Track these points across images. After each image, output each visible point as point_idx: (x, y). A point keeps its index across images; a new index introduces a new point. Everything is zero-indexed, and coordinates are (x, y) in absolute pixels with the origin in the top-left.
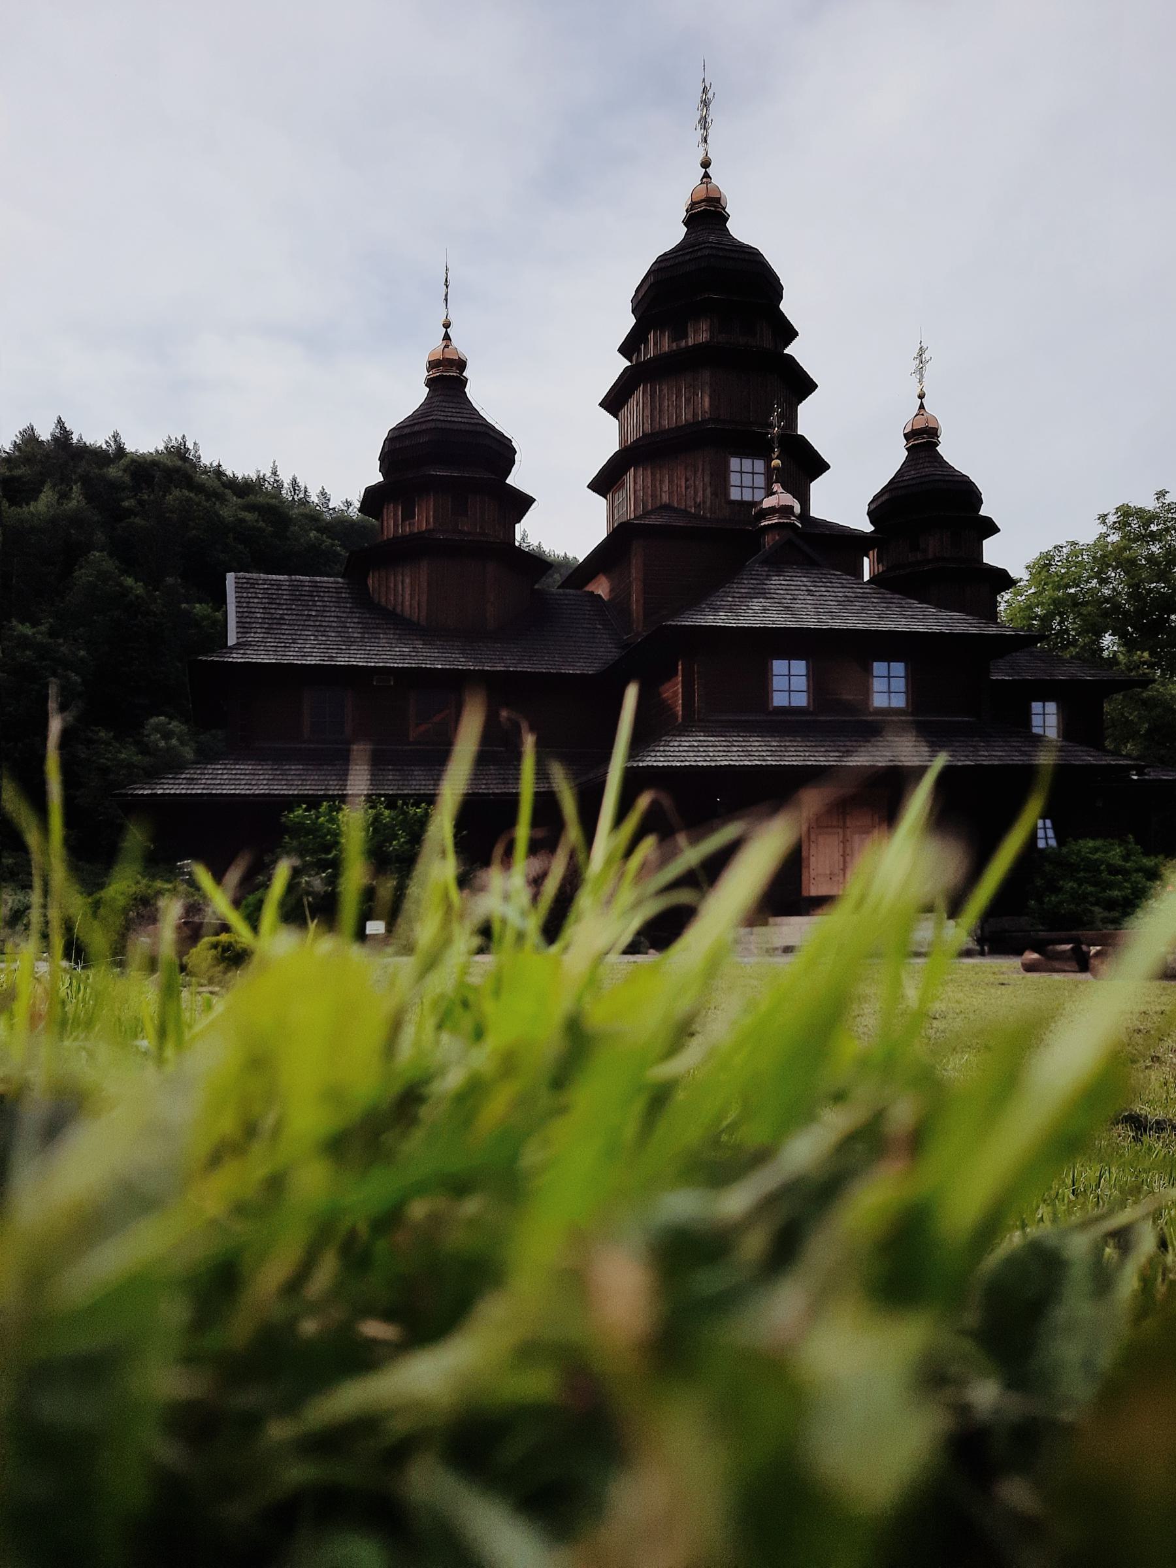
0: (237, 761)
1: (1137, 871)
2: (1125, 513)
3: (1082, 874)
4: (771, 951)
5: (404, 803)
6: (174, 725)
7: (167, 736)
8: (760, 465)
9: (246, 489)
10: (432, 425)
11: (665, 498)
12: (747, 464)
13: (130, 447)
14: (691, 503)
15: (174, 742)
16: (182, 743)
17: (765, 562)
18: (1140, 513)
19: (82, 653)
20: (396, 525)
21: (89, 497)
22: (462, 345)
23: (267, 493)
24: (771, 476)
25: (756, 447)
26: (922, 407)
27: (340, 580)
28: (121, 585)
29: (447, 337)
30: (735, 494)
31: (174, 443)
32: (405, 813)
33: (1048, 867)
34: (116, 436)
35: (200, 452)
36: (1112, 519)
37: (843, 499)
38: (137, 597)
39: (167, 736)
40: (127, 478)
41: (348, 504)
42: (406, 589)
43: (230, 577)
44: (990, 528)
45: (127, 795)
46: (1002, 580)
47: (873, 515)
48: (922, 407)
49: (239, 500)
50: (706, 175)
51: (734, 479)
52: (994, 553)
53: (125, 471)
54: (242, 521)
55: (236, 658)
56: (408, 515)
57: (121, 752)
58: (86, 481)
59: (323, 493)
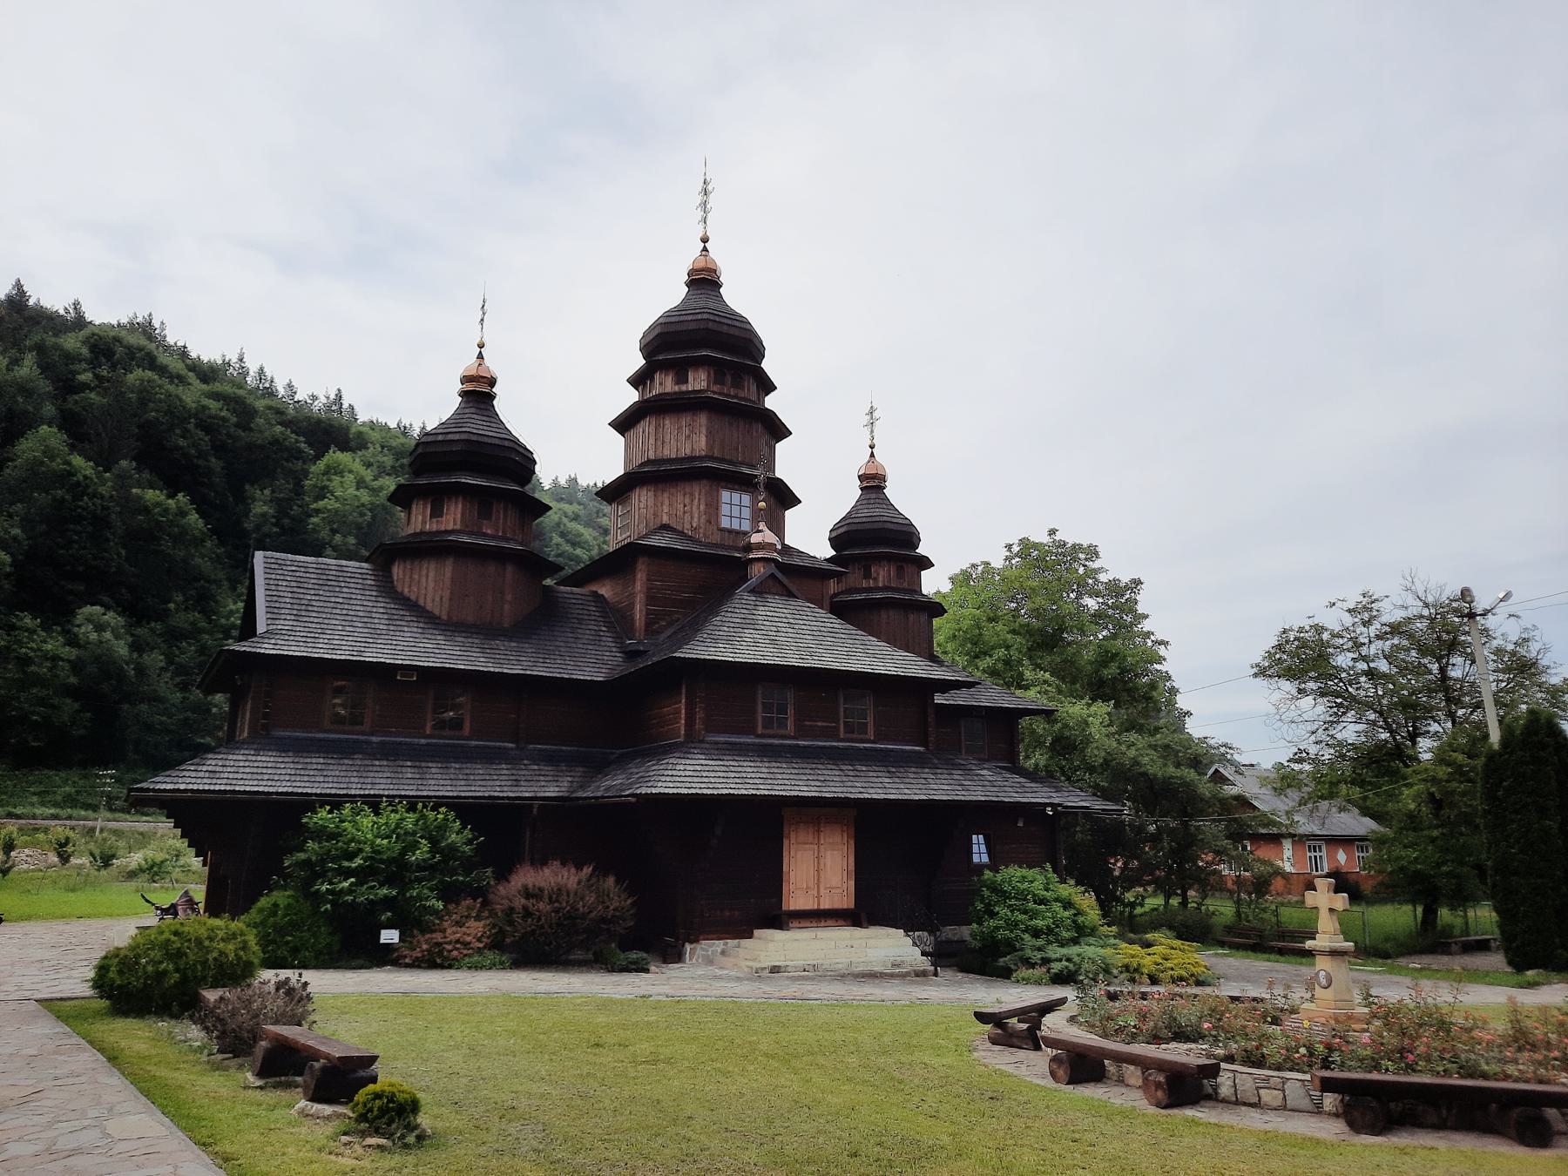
0: (258, 751)
1: (1056, 900)
2: (1026, 544)
3: (1013, 902)
4: (757, 975)
5: (425, 806)
6: (111, 617)
7: (100, 628)
8: (746, 499)
9: (208, 373)
10: (464, 437)
11: (665, 520)
12: (736, 496)
13: (89, 317)
14: (687, 526)
15: (108, 635)
16: (117, 637)
17: (752, 591)
18: (1036, 546)
19: (16, 531)
20: (424, 522)
21: (45, 367)
22: (493, 365)
23: (232, 382)
24: (756, 516)
25: (744, 483)
26: (872, 455)
27: (365, 565)
28: (68, 463)
29: (480, 356)
30: (725, 523)
31: (140, 320)
32: (423, 817)
33: (986, 893)
34: (76, 305)
35: (166, 332)
36: (1016, 549)
37: (809, 533)
38: (86, 477)
39: (100, 628)
40: (85, 351)
41: (314, 398)
42: (429, 582)
43: (259, 557)
44: (925, 563)
45: (148, 790)
46: (934, 608)
47: (835, 541)
48: (872, 455)
49: (204, 387)
50: (705, 249)
51: (725, 509)
52: (933, 583)
53: (84, 343)
54: (204, 408)
55: (267, 648)
56: (437, 513)
57: (45, 642)
58: (40, 349)
59: (290, 386)
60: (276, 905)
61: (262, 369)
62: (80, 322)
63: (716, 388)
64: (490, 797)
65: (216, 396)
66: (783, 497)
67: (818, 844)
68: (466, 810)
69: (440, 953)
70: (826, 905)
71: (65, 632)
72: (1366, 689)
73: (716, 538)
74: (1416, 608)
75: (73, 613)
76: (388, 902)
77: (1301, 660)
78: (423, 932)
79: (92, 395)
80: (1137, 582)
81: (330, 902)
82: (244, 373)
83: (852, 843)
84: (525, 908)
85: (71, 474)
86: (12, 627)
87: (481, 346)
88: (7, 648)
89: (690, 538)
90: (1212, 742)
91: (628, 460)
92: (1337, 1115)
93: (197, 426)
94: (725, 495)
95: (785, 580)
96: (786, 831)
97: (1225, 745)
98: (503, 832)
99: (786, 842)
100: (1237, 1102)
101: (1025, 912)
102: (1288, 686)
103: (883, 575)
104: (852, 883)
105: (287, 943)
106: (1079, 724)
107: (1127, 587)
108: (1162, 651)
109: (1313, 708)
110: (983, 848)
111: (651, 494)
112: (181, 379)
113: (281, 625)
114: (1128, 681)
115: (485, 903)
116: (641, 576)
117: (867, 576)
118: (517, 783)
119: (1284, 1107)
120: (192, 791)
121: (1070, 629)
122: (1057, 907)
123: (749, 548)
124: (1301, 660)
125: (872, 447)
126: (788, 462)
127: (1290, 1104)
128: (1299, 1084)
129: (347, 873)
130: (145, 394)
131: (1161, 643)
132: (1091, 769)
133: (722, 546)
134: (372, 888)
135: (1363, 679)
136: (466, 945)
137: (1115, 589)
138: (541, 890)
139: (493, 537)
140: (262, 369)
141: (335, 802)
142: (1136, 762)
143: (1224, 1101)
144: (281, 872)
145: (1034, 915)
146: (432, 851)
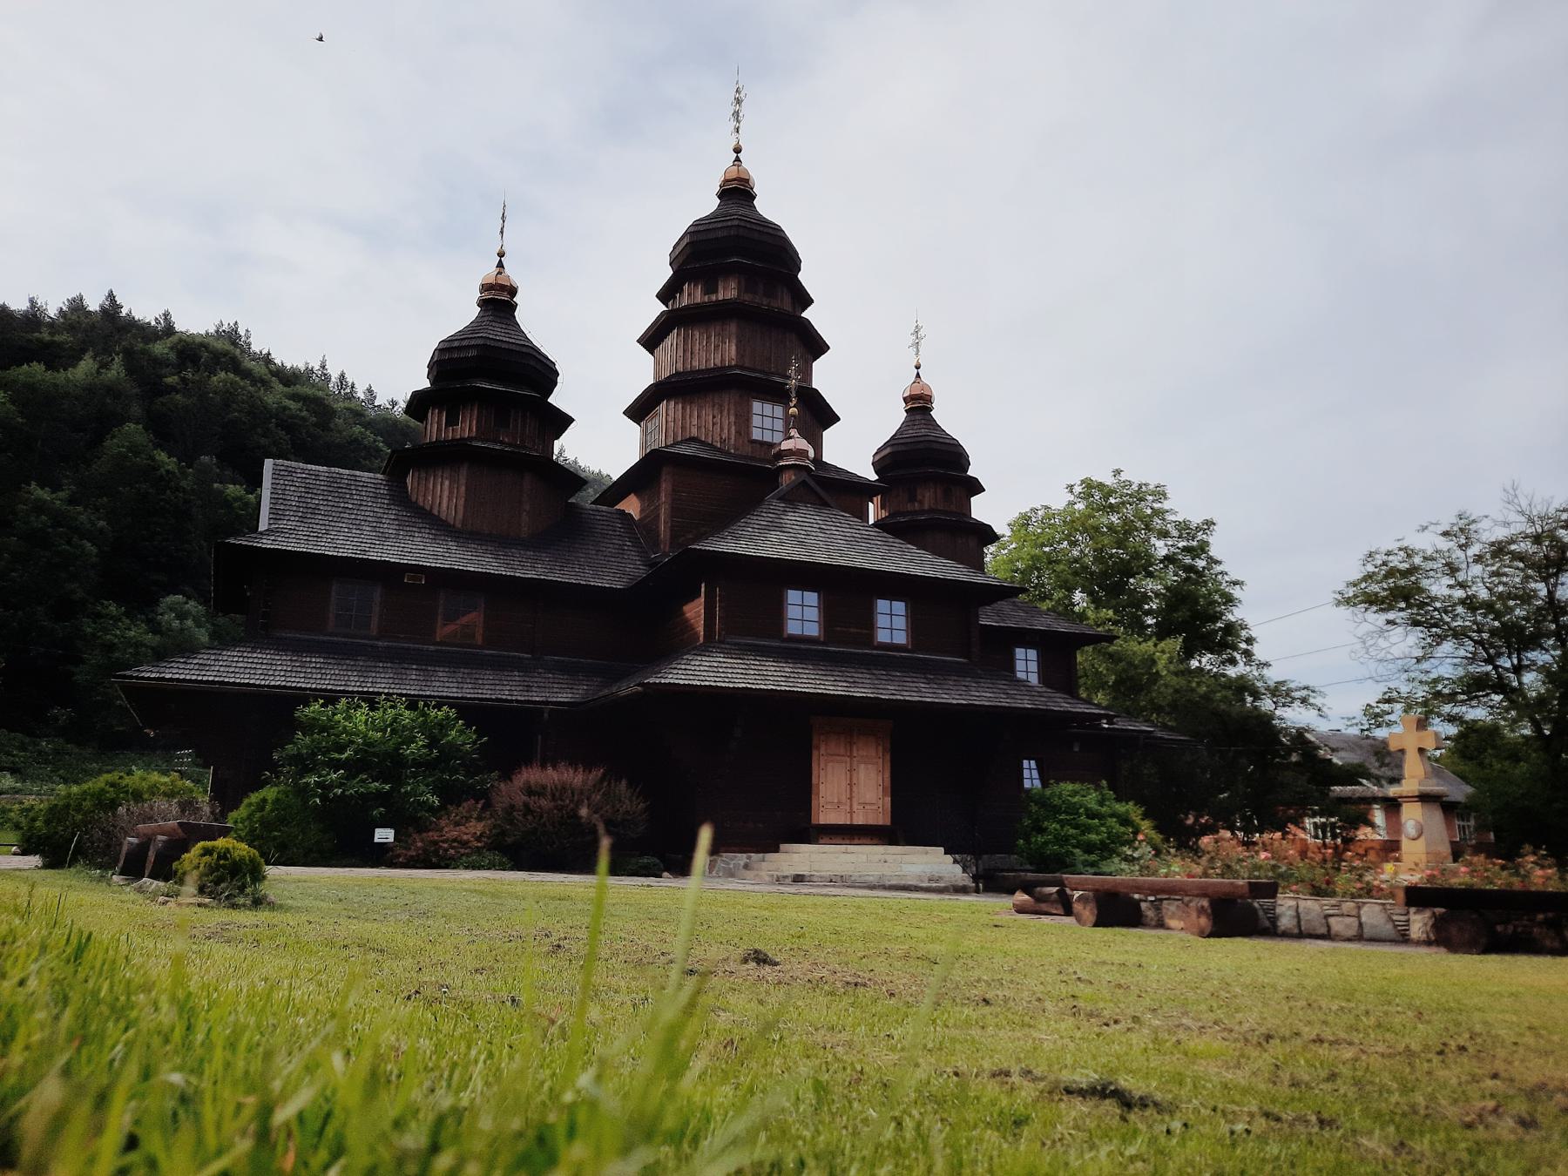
1: (1112, 816)
2: (1089, 485)
6: (192, 606)
9: (289, 378)
10: (479, 342)
11: (694, 432)
12: (768, 408)
13: (179, 327)
15: (189, 623)
17: (782, 499)
19: (102, 523)
22: (514, 274)
25: (777, 394)
26: (918, 375)
27: (379, 476)
28: (152, 458)
29: (500, 265)
30: (756, 435)
31: (225, 327)
32: (424, 715)
34: (166, 315)
36: (1078, 489)
37: (853, 448)
39: (182, 616)
40: (172, 356)
41: (394, 403)
42: (444, 493)
43: (268, 464)
45: (131, 677)
46: (986, 535)
47: (878, 466)
48: (918, 375)
50: (738, 159)
51: (756, 421)
52: (980, 509)
53: (171, 348)
54: (285, 408)
55: (266, 543)
56: (452, 421)
58: (129, 354)
59: (370, 391)
60: (264, 800)
61: (342, 376)
62: (169, 330)
63: (747, 297)
64: (497, 700)
65: (295, 397)
66: (818, 415)
67: (851, 757)
68: (469, 711)
69: (436, 853)
70: (859, 820)
71: (149, 621)
72: (1463, 618)
73: (748, 450)
74: (1520, 526)
75: (156, 603)
76: (380, 797)
77: (1394, 590)
78: (419, 832)
79: (178, 397)
80: (1209, 523)
81: (320, 796)
82: (327, 378)
83: (888, 757)
84: (526, 805)
85: (156, 469)
86: (99, 615)
87: (918, 367)
88: (93, 635)
89: (719, 450)
90: (1292, 686)
91: (657, 373)
92: (1428, 943)
93: (277, 425)
94: (757, 406)
95: (818, 489)
96: (815, 742)
97: (1306, 688)
98: (509, 735)
99: (815, 753)
100: (1300, 934)
101: (1076, 827)
102: (1376, 619)
103: (928, 498)
104: (814, 781)
105: (275, 838)
106: (1143, 661)
107: (1198, 529)
108: (1236, 592)
109: (1405, 641)
110: (1035, 774)
111: (672, 403)
112: (264, 383)
113: (282, 524)
114: (1199, 614)
115: (488, 805)
116: (665, 486)
117: (912, 499)
118: (528, 688)
119: (1359, 937)
120: (178, 680)
121: (1144, 586)
122: (1112, 821)
123: (782, 455)
124: (1394, 590)
125: (918, 367)
126: (825, 377)
127: (1367, 932)
128: (1378, 908)
129: (336, 765)
130: (229, 396)
131: (1235, 583)
132: (1159, 709)
133: (752, 458)
134: (363, 781)
135: (1460, 609)
136: (465, 844)
137: (1184, 528)
138: (544, 787)
139: (510, 445)
140: (342, 376)
141: (331, 698)
142: (1206, 697)
143: (1286, 935)
144: (274, 767)
145: (1088, 829)
146: (429, 746)
